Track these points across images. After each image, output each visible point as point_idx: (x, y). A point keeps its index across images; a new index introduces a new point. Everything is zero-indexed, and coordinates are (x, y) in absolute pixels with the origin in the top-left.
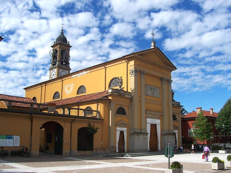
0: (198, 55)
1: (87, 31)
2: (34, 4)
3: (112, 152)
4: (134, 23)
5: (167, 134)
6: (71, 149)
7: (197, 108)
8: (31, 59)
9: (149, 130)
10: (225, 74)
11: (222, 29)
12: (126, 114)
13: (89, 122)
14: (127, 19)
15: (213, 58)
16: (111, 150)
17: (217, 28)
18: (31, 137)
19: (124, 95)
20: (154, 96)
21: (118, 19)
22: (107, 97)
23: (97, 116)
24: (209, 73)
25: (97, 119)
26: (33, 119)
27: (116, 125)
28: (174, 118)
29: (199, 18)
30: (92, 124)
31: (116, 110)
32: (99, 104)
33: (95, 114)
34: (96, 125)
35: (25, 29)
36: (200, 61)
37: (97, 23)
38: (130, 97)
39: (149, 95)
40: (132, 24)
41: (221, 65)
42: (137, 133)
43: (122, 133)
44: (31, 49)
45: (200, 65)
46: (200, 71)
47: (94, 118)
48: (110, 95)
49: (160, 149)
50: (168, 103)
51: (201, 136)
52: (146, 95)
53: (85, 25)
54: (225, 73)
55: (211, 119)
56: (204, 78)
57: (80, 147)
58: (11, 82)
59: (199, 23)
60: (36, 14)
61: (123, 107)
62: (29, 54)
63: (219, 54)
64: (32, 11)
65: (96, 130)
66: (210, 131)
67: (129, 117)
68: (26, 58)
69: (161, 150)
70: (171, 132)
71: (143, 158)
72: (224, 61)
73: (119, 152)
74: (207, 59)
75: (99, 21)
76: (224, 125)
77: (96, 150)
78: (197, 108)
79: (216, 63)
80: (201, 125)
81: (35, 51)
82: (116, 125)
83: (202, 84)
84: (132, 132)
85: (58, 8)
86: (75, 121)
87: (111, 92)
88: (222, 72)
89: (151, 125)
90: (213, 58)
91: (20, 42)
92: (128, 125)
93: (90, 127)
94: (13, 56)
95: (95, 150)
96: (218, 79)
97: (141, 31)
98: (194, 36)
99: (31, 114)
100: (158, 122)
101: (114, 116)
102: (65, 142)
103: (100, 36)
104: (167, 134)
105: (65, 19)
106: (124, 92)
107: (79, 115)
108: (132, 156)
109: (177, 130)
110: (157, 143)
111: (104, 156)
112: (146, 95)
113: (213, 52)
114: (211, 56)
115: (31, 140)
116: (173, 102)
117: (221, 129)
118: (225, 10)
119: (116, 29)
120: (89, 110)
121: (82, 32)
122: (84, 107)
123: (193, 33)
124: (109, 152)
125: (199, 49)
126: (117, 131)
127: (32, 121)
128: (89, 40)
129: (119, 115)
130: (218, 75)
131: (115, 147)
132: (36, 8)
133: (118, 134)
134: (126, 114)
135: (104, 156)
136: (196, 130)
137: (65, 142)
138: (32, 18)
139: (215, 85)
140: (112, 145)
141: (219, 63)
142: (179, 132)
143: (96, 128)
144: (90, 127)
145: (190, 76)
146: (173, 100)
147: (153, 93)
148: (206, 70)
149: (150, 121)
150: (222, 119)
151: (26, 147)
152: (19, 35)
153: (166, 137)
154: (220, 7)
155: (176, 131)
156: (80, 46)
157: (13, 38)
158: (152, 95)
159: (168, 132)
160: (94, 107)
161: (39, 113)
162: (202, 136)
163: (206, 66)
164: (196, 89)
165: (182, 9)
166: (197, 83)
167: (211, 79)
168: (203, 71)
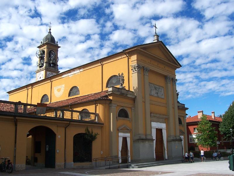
0: (194, 62)
1: (88, 37)
2: (36, 11)
3: (114, 163)
4: (135, 31)
5: (173, 140)
6: (65, 161)
7: (198, 112)
8: (26, 67)
9: (154, 137)
10: (219, 80)
11: (222, 36)
12: (128, 118)
13: (87, 127)
14: (128, 26)
15: (209, 65)
16: (114, 160)
17: (217, 35)
18: (15, 146)
19: (127, 95)
20: (158, 97)
21: (120, 26)
22: (107, 96)
23: (95, 120)
24: (203, 80)
25: (96, 123)
26: (18, 123)
27: (118, 130)
28: (180, 122)
29: (199, 26)
30: (90, 130)
31: (118, 114)
32: (97, 105)
33: (92, 117)
34: (95, 131)
35: (23, 36)
36: (196, 68)
37: (98, 31)
38: (133, 97)
39: (153, 96)
40: (133, 31)
41: (216, 71)
42: (143, 139)
43: (125, 139)
44: (27, 57)
45: (196, 72)
46: (194, 78)
47: (92, 122)
48: (110, 95)
49: (166, 157)
50: (173, 104)
51: (205, 142)
52: (151, 95)
53: (86, 33)
54: (219, 80)
55: (215, 124)
56: (197, 85)
57: (77, 158)
58: (3, 90)
59: (199, 31)
60: (37, 20)
61: (125, 109)
62: (25, 62)
63: (215, 61)
64: (32, 17)
65: (95, 137)
66: (215, 136)
67: (132, 120)
68: (20, 66)
69: (168, 159)
70: (178, 138)
71: (154, 169)
72: (219, 68)
73: (122, 163)
74: (203, 67)
75: (101, 28)
76: (231, 129)
77: (96, 160)
78: (198, 112)
79: (211, 70)
80: (205, 130)
81: (30, 59)
82: (118, 130)
83: (195, 91)
84: (137, 137)
85: (61, 14)
86: (70, 125)
87: (112, 91)
88: (217, 79)
89: (157, 129)
90: (209, 65)
91: (16, 49)
92: (131, 130)
93: (88, 133)
94: (7, 64)
95: (95, 161)
96: (211, 86)
97: (142, 39)
98: (190, 44)
99: (15, 116)
100: (163, 126)
101: (116, 120)
102: (58, 152)
103: (100, 43)
104: (173, 140)
105: (66, 25)
106: (126, 91)
107: (73, 119)
108: (139, 167)
109: (183, 135)
110: (162, 150)
111: (106, 169)
112: (151, 95)
113: (210, 59)
114: (207, 63)
115: (15, 151)
116: (178, 104)
117: (227, 134)
118: (225, 18)
119: (117, 36)
120: (85, 113)
121: (83, 38)
122: (80, 109)
123: (193, 39)
124: (111, 162)
125: (196, 56)
126: (120, 138)
127: (16, 125)
128: (88, 47)
129: (121, 118)
130: (212, 82)
131: (117, 157)
132: (37, 15)
133: (121, 140)
134: (128, 118)
135: (106, 169)
136: (199, 135)
137: (58, 152)
138: (32, 24)
139: (208, 92)
140: (114, 154)
141: (214, 70)
142: (185, 138)
143: (95, 134)
144: (88, 133)
145: (185, 83)
146: (178, 102)
147: (157, 93)
148: (200, 76)
149: (121, 135)
150: (228, 123)
151: (9, 159)
152: (17, 43)
153: (173, 143)
154: (221, 15)
155: (182, 137)
156: (77, 53)
157: (10, 45)
158: (156, 95)
159: (175, 138)
160: (91, 108)
161: (26, 116)
162: (207, 141)
163: (201, 73)
164: (190, 96)
165: (185, 16)
166: (190, 89)
167: (205, 85)
168: (197, 77)
